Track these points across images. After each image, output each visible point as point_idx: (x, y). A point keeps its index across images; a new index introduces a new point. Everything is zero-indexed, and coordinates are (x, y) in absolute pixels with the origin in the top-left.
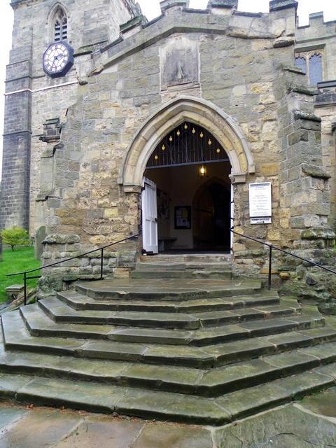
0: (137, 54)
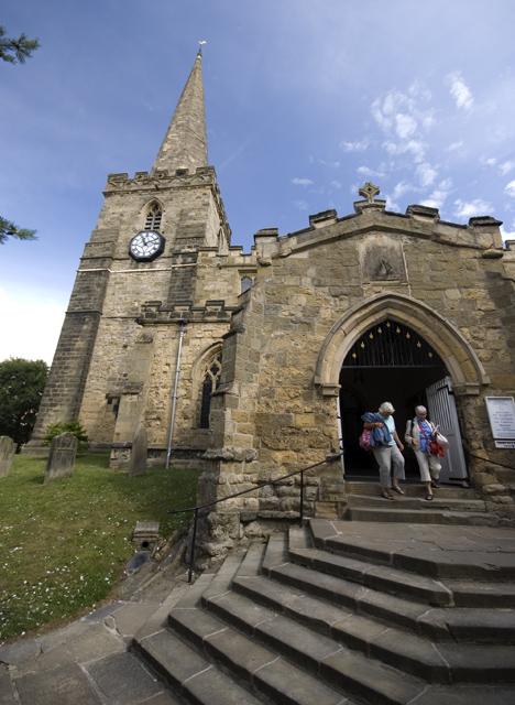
0: (331, 245)
